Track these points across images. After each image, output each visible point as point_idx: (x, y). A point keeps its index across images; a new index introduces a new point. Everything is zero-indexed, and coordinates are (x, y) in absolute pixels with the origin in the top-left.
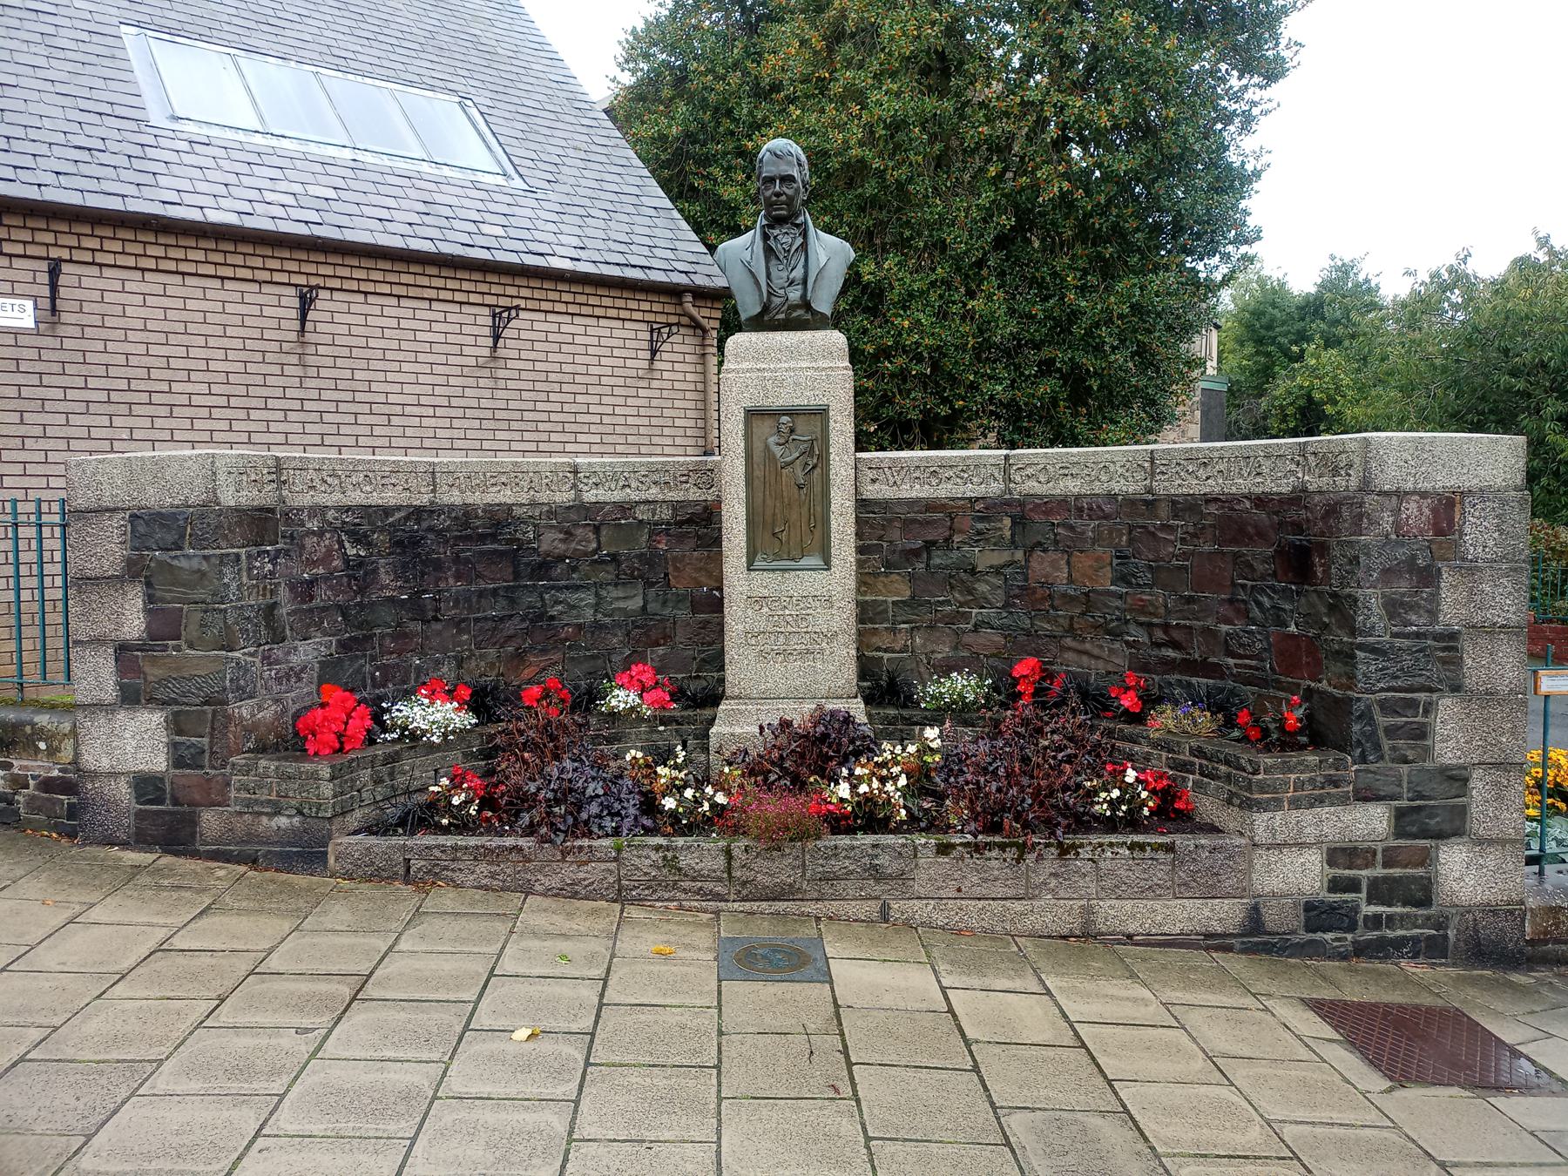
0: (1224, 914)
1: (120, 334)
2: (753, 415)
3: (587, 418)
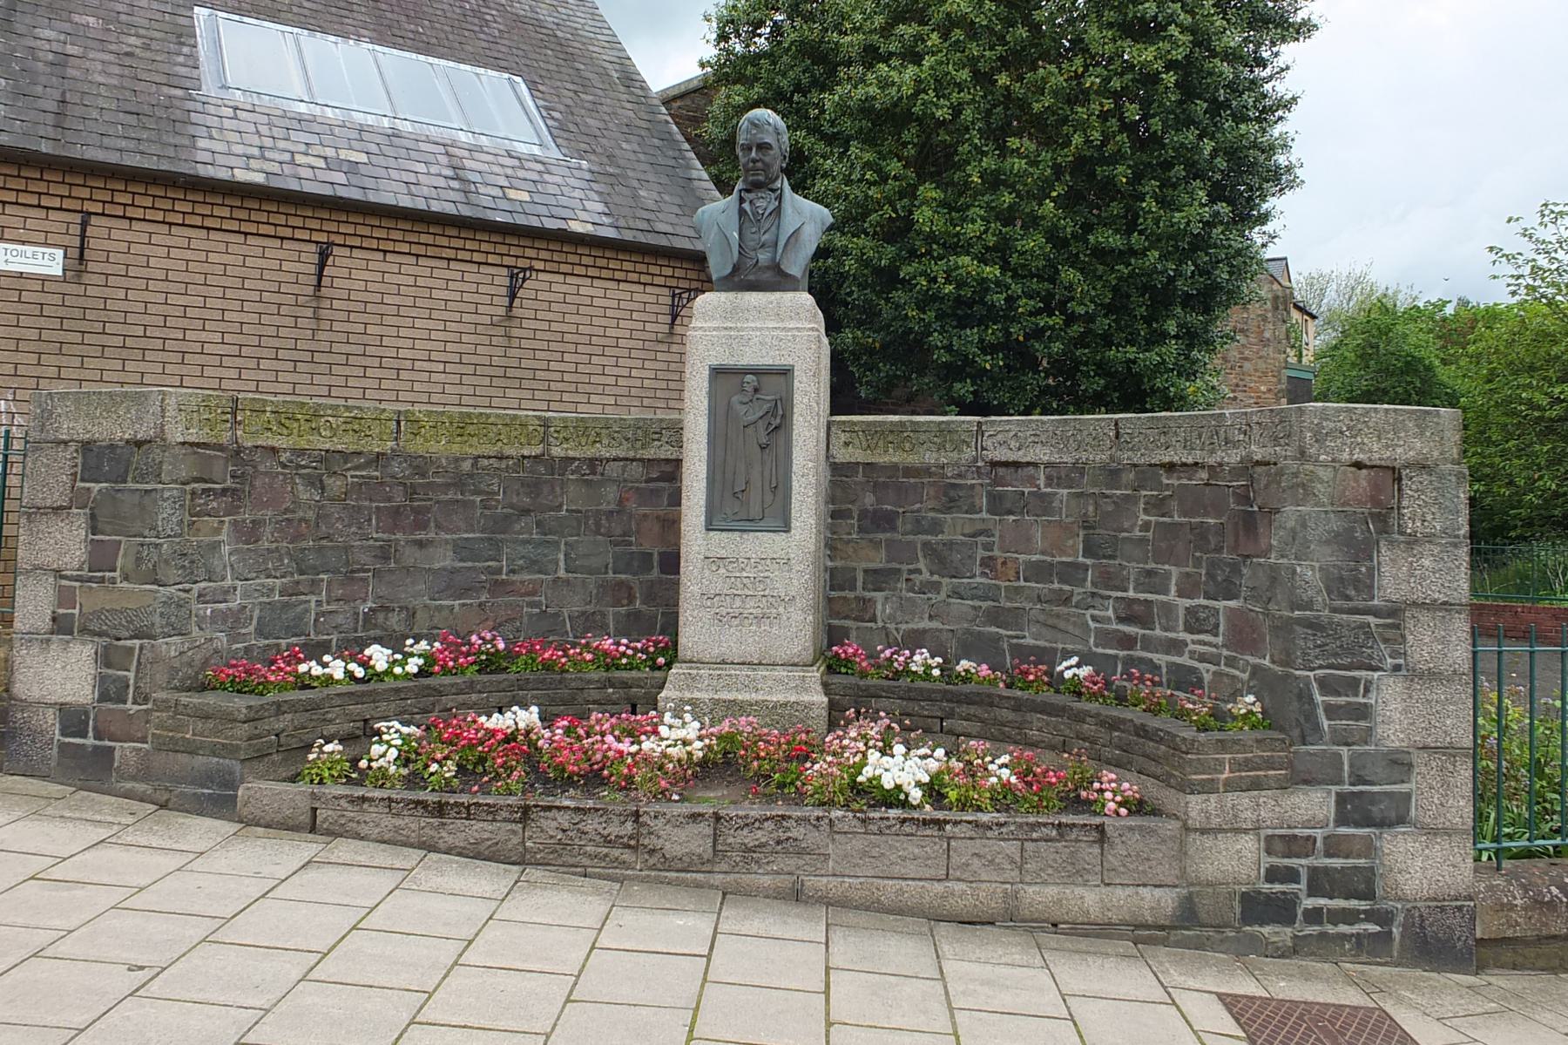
0: (1160, 901)
1: (142, 284)
2: (718, 372)
3: (602, 380)
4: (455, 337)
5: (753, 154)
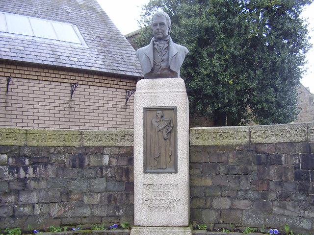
2: (147, 110)
3: (103, 122)
4: (53, 108)
5: (158, 27)
